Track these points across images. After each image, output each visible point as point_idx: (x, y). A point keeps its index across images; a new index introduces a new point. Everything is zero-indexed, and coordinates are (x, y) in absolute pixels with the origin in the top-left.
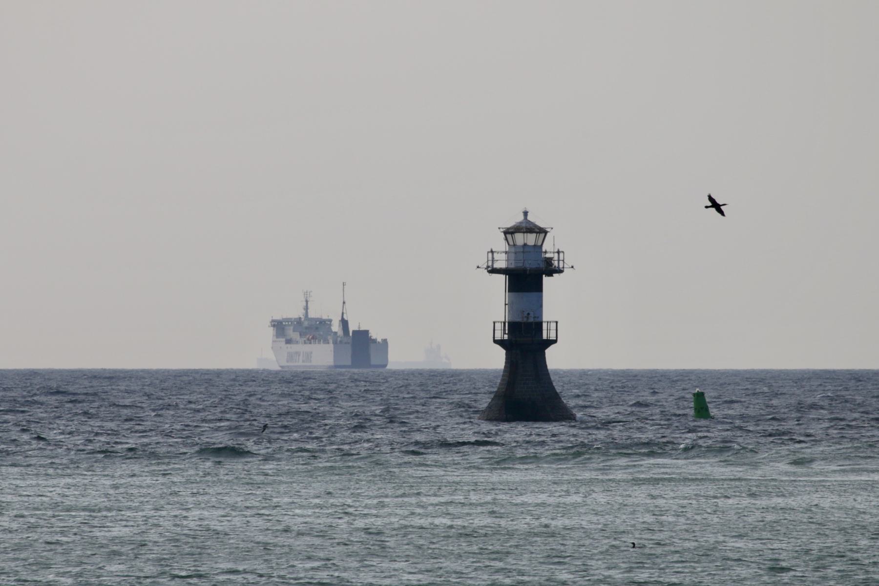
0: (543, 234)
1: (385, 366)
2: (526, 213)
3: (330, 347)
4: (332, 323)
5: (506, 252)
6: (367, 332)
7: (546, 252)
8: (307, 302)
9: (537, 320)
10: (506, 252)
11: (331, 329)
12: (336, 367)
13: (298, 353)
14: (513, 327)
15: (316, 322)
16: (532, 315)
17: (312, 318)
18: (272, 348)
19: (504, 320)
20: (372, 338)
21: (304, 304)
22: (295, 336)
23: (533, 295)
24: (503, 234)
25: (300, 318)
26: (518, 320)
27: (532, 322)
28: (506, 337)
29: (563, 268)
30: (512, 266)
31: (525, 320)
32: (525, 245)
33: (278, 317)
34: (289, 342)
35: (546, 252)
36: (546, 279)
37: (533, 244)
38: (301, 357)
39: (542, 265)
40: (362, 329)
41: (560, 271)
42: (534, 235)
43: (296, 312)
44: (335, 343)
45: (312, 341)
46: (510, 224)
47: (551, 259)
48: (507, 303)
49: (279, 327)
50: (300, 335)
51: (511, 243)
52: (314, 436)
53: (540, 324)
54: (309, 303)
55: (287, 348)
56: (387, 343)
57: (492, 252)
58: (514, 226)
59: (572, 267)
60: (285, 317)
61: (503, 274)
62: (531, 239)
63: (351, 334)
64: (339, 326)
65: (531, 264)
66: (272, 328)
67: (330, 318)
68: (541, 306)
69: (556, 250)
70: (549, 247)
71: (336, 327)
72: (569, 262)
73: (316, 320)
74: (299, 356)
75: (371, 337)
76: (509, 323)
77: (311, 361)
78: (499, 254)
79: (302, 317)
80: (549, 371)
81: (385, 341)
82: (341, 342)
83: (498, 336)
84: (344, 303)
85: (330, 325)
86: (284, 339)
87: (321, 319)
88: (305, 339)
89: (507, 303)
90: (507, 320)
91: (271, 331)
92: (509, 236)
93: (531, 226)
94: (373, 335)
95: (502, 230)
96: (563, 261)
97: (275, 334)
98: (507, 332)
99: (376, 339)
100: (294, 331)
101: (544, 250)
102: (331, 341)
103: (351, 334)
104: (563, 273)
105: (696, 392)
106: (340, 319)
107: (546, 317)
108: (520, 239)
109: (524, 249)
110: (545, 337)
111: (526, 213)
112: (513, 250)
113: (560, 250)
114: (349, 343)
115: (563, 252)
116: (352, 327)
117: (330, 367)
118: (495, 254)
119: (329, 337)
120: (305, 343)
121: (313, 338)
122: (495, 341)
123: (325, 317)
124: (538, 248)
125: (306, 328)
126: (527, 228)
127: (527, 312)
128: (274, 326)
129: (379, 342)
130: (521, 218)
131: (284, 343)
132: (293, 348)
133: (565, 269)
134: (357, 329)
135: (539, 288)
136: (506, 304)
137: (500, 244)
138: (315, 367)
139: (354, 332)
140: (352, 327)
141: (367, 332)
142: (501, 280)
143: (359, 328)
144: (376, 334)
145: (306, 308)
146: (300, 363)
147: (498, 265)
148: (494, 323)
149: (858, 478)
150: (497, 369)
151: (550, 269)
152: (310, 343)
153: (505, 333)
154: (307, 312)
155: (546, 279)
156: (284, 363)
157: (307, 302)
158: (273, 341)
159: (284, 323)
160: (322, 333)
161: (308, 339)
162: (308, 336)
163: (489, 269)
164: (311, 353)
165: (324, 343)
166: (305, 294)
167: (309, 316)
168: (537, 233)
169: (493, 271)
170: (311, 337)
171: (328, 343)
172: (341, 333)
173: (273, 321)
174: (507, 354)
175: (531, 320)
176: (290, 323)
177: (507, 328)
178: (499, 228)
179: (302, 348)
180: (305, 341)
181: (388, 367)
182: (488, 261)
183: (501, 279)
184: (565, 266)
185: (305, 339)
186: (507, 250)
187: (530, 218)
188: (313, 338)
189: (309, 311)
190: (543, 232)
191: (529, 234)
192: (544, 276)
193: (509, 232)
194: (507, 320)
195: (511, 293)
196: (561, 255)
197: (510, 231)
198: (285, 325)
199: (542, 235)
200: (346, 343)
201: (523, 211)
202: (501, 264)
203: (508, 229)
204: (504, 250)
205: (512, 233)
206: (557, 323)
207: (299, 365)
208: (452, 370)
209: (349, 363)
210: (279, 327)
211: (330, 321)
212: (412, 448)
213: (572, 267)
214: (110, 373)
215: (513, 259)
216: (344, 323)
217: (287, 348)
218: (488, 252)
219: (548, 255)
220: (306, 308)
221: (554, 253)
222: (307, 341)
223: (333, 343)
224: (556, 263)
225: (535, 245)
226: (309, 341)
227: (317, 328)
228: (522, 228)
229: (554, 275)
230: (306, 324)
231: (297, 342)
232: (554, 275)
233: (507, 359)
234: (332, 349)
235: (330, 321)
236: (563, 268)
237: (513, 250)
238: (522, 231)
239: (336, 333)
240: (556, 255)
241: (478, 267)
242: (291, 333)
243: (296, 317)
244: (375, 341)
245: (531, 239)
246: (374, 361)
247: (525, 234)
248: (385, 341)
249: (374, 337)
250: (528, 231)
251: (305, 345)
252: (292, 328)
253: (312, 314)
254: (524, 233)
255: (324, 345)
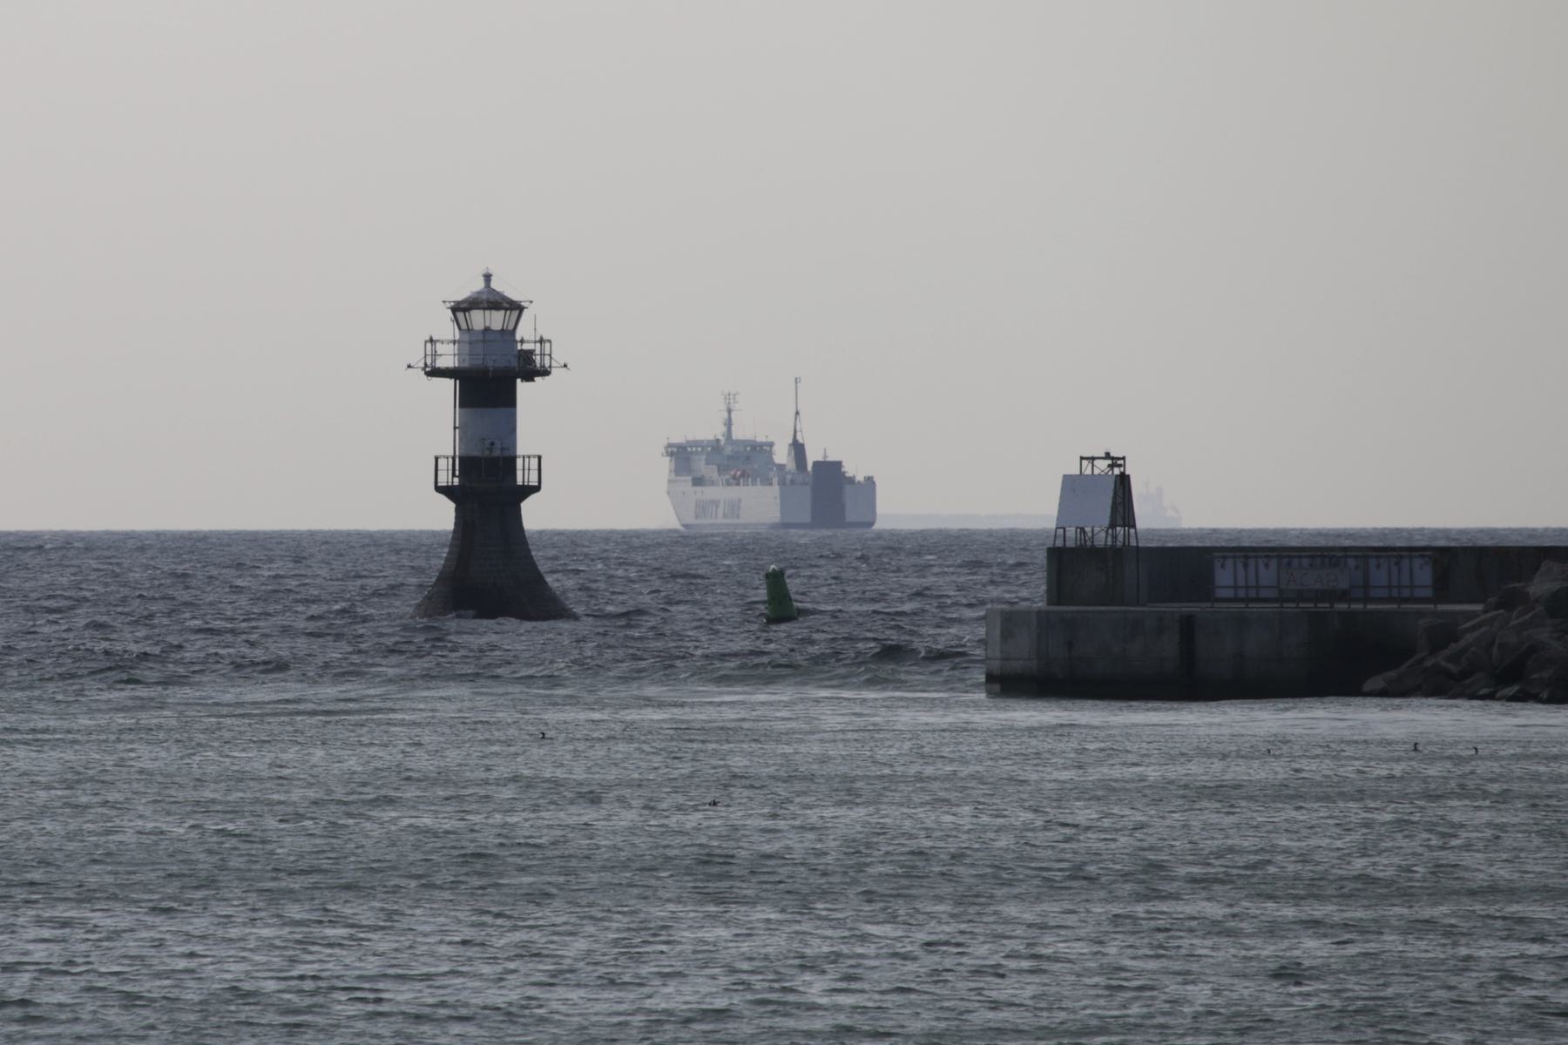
0: (517, 312)
1: (871, 524)
2: (488, 277)
3: (775, 489)
4: (775, 448)
5: (454, 342)
6: (838, 464)
7: (522, 341)
8: (729, 411)
9: (507, 454)
10: (454, 342)
11: (772, 459)
12: (786, 526)
13: (715, 503)
14: (468, 465)
15: (746, 447)
16: (498, 444)
17: (737, 441)
18: (668, 493)
19: (452, 454)
20: (847, 475)
21: (725, 415)
22: (711, 472)
23: (502, 411)
24: (450, 311)
25: (718, 440)
26: (476, 453)
27: (498, 458)
28: (456, 481)
29: (550, 367)
30: (466, 365)
31: (487, 453)
32: (487, 330)
33: (678, 439)
34: (698, 482)
35: (522, 341)
36: (522, 387)
37: (499, 328)
38: (720, 510)
39: (515, 363)
40: (831, 458)
41: (545, 372)
42: (502, 312)
43: (708, 429)
44: (782, 483)
45: (741, 481)
46: (462, 295)
47: (531, 352)
48: (457, 425)
49: (681, 455)
50: (719, 470)
51: (464, 326)
52: (631, 651)
53: (512, 460)
54: (733, 414)
55: (695, 493)
56: (874, 483)
57: (431, 340)
58: (470, 297)
59: (565, 366)
60: (690, 438)
61: (451, 377)
62: (496, 320)
63: (810, 468)
64: (789, 454)
65: (496, 361)
66: (668, 458)
67: (770, 440)
68: (514, 430)
69: (538, 339)
70: (526, 332)
71: (782, 455)
72: (559, 356)
73: (745, 443)
74: (717, 507)
75: (844, 472)
76: (460, 458)
77: (738, 517)
78: (445, 346)
79: (720, 437)
80: (527, 534)
81: (870, 481)
82: (792, 482)
83: (444, 480)
84: (797, 413)
85: (771, 453)
86: (690, 478)
87: (755, 441)
88: (727, 477)
89: (457, 425)
90: (457, 454)
91: (666, 464)
92: (460, 315)
93: (497, 298)
94: (849, 469)
95: (449, 305)
96: (550, 355)
97: (673, 468)
98: (457, 473)
99: (854, 477)
100: (708, 463)
101: (518, 337)
102: (775, 481)
103: (810, 468)
104: (551, 376)
105: (771, 570)
106: (791, 441)
107: (522, 448)
108: (478, 319)
109: (484, 336)
110: (519, 481)
111: (488, 277)
112: (467, 337)
113: (545, 338)
114: (806, 484)
115: (550, 341)
116: (813, 456)
117: (774, 526)
118: (439, 346)
119: (771, 474)
120: (728, 484)
121: (743, 475)
122: (439, 489)
123: (761, 439)
124: (508, 334)
125: (729, 458)
126: (489, 302)
127: (490, 441)
128: (671, 454)
129: (859, 482)
130: (479, 285)
131: (690, 484)
132: (708, 493)
133: (553, 370)
134: (820, 458)
135: (510, 401)
136: (455, 428)
137: (446, 328)
138: (745, 526)
139: (816, 464)
140: (813, 456)
141: (838, 464)
142: (447, 388)
143: (825, 456)
144: (855, 469)
145: (729, 423)
146: (720, 520)
147: (442, 363)
148: (437, 459)
149: (926, 718)
150: (414, 531)
151: (530, 368)
152: (738, 484)
153: (454, 475)
154: (729, 430)
155: (522, 387)
156: (691, 520)
157: (729, 411)
158: (670, 481)
159: (689, 449)
160: (756, 466)
161: (734, 477)
162: (732, 473)
163: (428, 369)
164: (740, 501)
165: (763, 483)
166: (725, 399)
167: (734, 437)
168: (506, 309)
169: (435, 372)
170: (739, 473)
171: (771, 484)
172: (791, 466)
173: (670, 445)
174: (457, 510)
175: (497, 453)
176: (700, 449)
177: (457, 467)
178: (444, 302)
179: (721, 493)
180: (727, 481)
181: (878, 526)
182: (426, 356)
183: (448, 386)
184: (554, 364)
185: (727, 477)
186: (457, 337)
187: (494, 285)
188: (743, 475)
189: (733, 428)
190: (516, 308)
191: (494, 312)
192: (519, 381)
193: (460, 309)
194: (457, 454)
195: (463, 410)
196: (547, 345)
197: (462, 306)
198: (692, 453)
199: (516, 313)
200: (801, 484)
201: (485, 272)
202: (447, 361)
203: (458, 303)
204: (452, 338)
205: (465, 310)
206: (540, 458)
207: (717, 521)
208: (1185, 530)
209: (807, 518)
210: (681, 455)
211: (771, 445)
212: (644, 674)
213: (565, 366)
214: (1448, 538)
215: (467, 352)
216: (798, 449)
217: (695, 493)
218: (426, 342)
219: (526, 347)
220: (729, 423)
221: (535, 342)
222: (731, 481)
223: (779, 484)
224: (538, 359)
225: (502, 330)
226: (736, 481)
227: (748, 458)
228: (482, 302)
229: (536, 379)
230: (728, 450)
231: (713, 483)
232: (536, 379)
233: (457, 517)
234: (778, 495)
235: (771, 445)
236: (550, 367)
237: (467, 337)
238: (482, 306)
239: (781, 467)
240: (538, 345)
241: (409, 366)
242: (701, 466)
243: (711, 437)
244: (851, 480)
245: (496, 320)
246: (851, 516)
247: (487, 312)
248: (870, 481)
249: (849, 474)
250: (491, 305)
251: (729, 487)
252: (704, 457)
253: (738, 434)
254: (484, 309)
255: (762, 487)
